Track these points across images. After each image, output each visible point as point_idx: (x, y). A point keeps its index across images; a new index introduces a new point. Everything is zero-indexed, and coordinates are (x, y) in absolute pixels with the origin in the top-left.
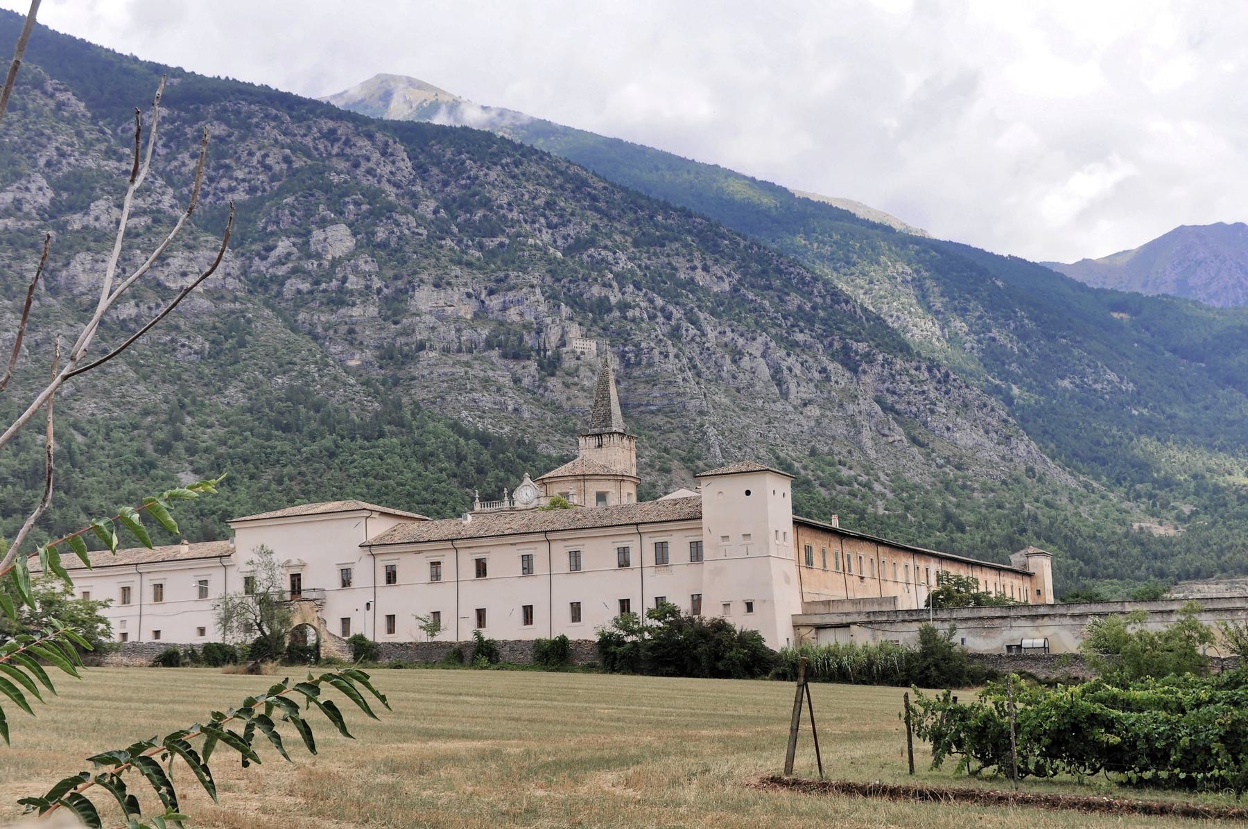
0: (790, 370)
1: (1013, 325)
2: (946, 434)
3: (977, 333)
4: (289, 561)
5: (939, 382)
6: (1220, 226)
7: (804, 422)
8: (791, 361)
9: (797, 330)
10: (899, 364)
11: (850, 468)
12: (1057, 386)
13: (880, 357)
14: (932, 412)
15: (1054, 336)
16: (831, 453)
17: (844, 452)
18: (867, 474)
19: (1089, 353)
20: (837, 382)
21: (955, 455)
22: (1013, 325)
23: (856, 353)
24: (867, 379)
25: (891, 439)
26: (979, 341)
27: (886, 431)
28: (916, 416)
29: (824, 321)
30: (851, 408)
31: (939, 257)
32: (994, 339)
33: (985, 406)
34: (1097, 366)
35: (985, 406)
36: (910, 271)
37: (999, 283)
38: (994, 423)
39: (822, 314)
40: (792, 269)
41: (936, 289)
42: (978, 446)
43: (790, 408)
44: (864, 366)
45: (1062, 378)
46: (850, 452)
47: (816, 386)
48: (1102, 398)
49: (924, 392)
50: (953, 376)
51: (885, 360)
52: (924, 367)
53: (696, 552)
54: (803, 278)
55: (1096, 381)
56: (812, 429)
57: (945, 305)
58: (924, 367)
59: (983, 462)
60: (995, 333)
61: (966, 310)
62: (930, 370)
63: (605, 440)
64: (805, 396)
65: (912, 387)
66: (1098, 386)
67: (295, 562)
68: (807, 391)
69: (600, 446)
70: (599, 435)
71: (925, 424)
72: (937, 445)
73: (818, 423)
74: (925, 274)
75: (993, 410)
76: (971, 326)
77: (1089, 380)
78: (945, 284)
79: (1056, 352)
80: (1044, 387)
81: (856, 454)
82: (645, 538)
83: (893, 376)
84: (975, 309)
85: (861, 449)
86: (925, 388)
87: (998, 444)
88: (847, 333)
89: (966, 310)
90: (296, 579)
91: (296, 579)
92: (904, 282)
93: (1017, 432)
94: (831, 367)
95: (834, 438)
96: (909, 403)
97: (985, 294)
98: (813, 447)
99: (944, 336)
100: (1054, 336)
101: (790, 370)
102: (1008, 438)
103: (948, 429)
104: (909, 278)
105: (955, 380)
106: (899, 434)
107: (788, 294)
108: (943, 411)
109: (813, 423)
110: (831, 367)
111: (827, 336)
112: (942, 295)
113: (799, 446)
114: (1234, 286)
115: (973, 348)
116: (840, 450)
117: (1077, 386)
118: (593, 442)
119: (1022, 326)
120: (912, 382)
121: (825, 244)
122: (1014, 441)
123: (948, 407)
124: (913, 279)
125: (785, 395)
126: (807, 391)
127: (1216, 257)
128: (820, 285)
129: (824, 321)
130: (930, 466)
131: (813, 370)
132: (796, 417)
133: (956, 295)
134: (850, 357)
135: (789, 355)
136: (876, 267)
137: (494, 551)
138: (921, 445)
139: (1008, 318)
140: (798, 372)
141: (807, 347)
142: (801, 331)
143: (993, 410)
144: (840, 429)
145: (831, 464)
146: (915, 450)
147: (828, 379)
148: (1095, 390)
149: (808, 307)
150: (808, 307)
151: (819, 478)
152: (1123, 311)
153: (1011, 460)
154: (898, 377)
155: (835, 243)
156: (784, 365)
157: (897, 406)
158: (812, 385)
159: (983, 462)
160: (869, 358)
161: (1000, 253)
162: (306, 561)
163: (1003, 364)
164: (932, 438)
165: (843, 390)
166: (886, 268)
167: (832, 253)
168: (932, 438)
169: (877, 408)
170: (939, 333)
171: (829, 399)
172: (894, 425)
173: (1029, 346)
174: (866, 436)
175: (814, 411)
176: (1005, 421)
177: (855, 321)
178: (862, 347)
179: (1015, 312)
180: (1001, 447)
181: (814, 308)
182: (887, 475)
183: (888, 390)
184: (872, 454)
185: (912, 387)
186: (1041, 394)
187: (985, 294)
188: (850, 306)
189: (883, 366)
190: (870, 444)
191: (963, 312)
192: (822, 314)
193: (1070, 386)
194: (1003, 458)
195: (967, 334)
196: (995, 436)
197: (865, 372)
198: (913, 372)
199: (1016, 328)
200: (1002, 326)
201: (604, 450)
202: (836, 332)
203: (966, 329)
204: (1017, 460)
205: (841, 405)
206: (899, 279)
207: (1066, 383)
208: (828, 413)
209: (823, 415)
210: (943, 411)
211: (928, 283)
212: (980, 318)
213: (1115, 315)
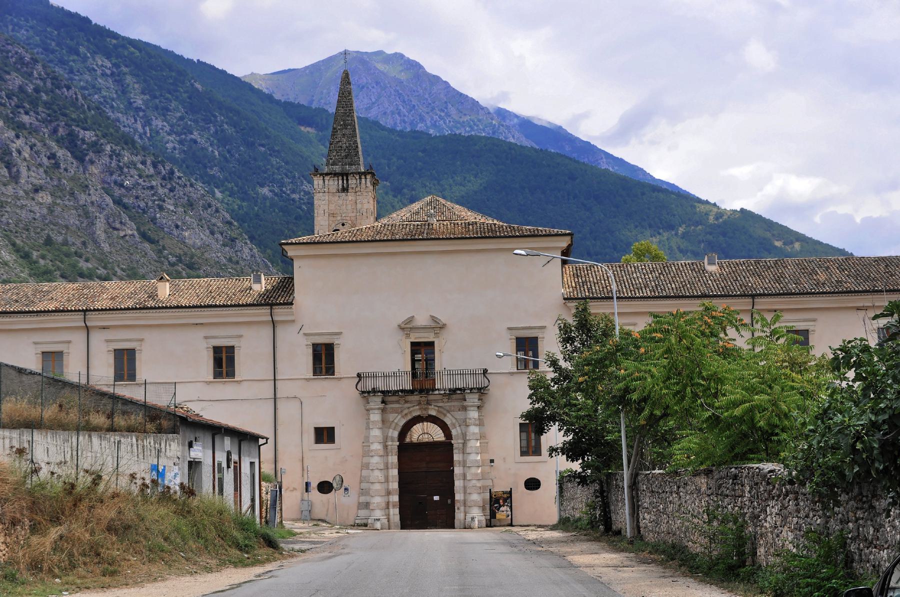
0: (19, 152)
1: (213, 129)
2: (175, 232)
3: (178, 134)
4: (411, 319)
5: (164, 178)
6: (223, 72)
7: (36, 208)
8: (19, 142)
9: (22, 111)
10: (127, 157)
11: (87, 260)
12: (257, 193)
13: (108, 148)
14: (161, 208)
15: (253, 144)
16: (65, 243)
17: (78, 243)
18: (105, 268)
19: (287, 163)
20: (66, 170)
21: (185, 254)
22: (213, 129)
23: (83, 140)
24: (94, 169)
25: (122, 234)
26: (181, 142)
27: (118, 226)
28: (144, 212)
29: (46, 105)
30: (83, 198)
31: (137, 54)
32: (195, 142)
33: (210, 206)
34: (294, 177)
35: (210, 206)
36: (109, 65)
37: (198, 86)
38: (220, 224)
39: (44, 97)
40: (10, 47)
41: (136, 86)
42: (205, 247)
43: (21, 193)
44: (91, 155)
45: (262, 186)
46: (84, 243)
47: (45, 172)
48: (300, 208)
49: (152, 188)
50: (177, 174)
51: (113, 151)
52: (149, 162)
53: (527, 345)
54: (22, 58)
55: (293, 192)
56: (44, 217)
57: (146, 103)
58: (149, 162)
59: (212, 262)
60: (195, 135)
61: (168, 110)
62: (155, 165)
63: (352, 182)
64: (36, 182)
65: (141, 181)
66: (295, 196)
67: (422, 320)
68: (37, 177)
69: (345, 190)
70: (344, 175)
71: (153, 220)
72: (167, 242)
73: (51, 210)
74: (125, 69)
75: (217, 211)
76: (172, 126)
77: (287, 189)
78: (145, 81)
79: (255, 159)
80: (245, 193)
81: (90, 248)
82: (97, 338)
83: (121, 168)
84: (176, 109)
85: (95, 242)
86: (154, 183)
87: (224, 245)
88: (73, 120)
89: (168, 110)
90: (422, 352)
91: (422, 352)
92: (104, 75)
93: (241, 234)
94: (61, 153)
95: (67, 227)
96: (137, 197)
97: (185, 95)
98: (48, 236)
99: (145, 133)
100: (253, 144)
101: (19, 152)
102: (233, 240)
103: (177, 227)
104: (108, 72)
105: (179, 178)
106: (130, 229)
107: (9, 73)
108: (172, 208)
109: (45, 211)
110: (61, 153)
111: (51, 121)
112: (143, 93)
113: (33, 234)
114: (393, 113)
115: (174, 148)
116: (76, 242)
117: (276, 194)
118: (333, 184)
119: (223, 131)
120: (140, 176)
121: (21, 27)
122: (239, 244)
123: (176, 205)
124: (113, 74)
125: (15, 178)
126: (37, 177)
127: (377, 83)
128: (39, 67)
129: (46, 105)
130: (162, 263)
131: (42, 156)
132: (29, 203)
133: (158, 94)
134: (76, 146)
135: (18, 137)
136: (76, 57)
137: (821, 317)
138: (151, 241)
139: (207, 121)
140: (27, 156)
141: (33, 131)
142: (27, 113)
143: (217, 211)
144: (72, 219)
145: (67, 255)
146: (147, 245)
147: (57, 166)
148: (293, 200)
149: (30, 89)
150: (30, 89)
151: (59, 269)
152: (309, 125)
153: (237, 263)
154: (126, 170)
155: (32, 27)
156: (13, 147)
157: (125, 200)
158: (41, 170)
159: (212, 262)
160: (97, 148)
161: (190, 57)
162: (443, 319)
163: (205, 167)
164: (162, 234)
165: (72, 179)
166: (85, 59)
167: (28, 39)
168: (162, 234)
169: (109, 200)
170: (140, 130)
171: (59, 187)
172: (125, 218)
173: (229, 152)
174: (100, 227)
175: (45, 198)
176: (230, 223)
177: (77, 108)
178: (89, 135)
179: (215, 117)
180: (227, 249)
181: (37, 90)
182: (122, 269)
183: (115, 182)
184: (106, 247)
185: (141, 181)
186: (243, 200)
187: (185, 95)
188: (71, 92)
189: (111, 157)
190: (103, 236)
191: (164, 111)
192: (44, 97)
193: (269, 195)
194: (230, 260)
195: (169, 134)
196: (220, 237)
197: (92, 162)
198: (140, 166)
199: (216, 132)
200: (203, 129)
201: (351, 196)
202: (61, 118)
203: (168, 128)
204: (242, 263)
205: (72, 194)
206: (99, 72)
207: (265, 191)
208: (58, 201)
209: (54, 203)
210: (172, 208)
211: (129, 79)
212: (181, 118)
213: (302, 128)
